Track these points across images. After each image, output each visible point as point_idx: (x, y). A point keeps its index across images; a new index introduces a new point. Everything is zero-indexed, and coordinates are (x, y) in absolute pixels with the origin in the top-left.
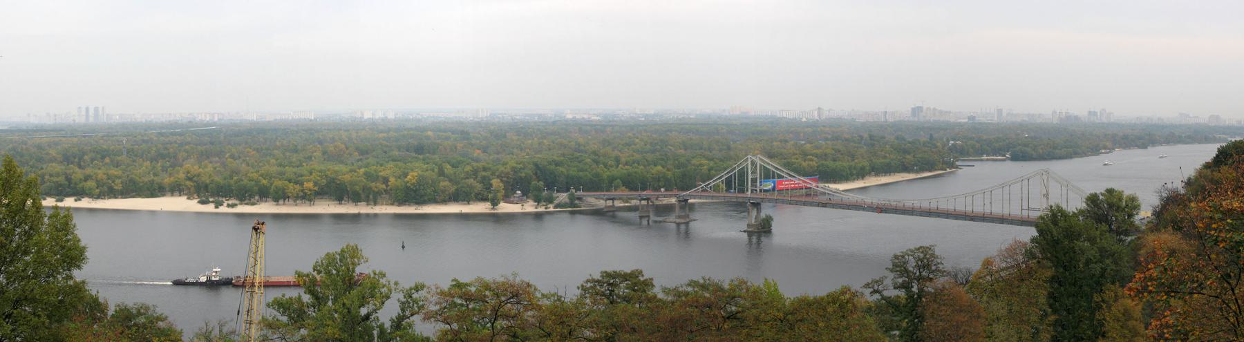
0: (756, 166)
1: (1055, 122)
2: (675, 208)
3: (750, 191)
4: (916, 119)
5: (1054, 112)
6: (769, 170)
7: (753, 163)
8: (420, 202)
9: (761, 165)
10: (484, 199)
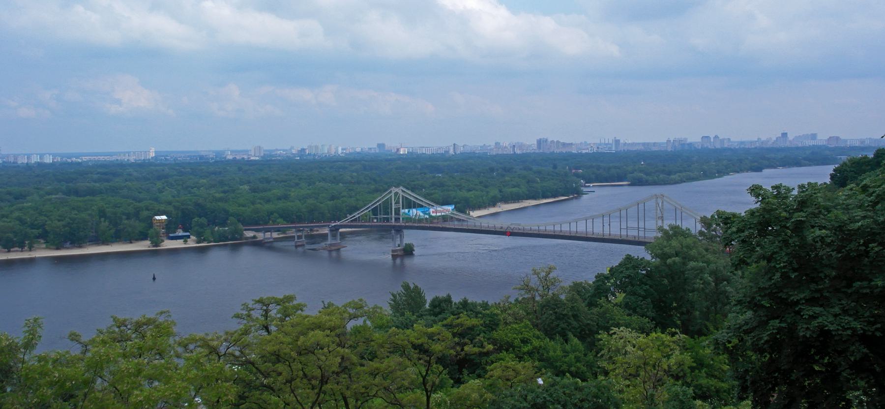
0: (399, 198)
1: (669, 149)
2: (328, 235)
3: (393, 219)
4: (541, 151)
5: (669, 141)
6: (411, 200)
8: (77, 242)
9: (403, 196)
10: (143, 237)
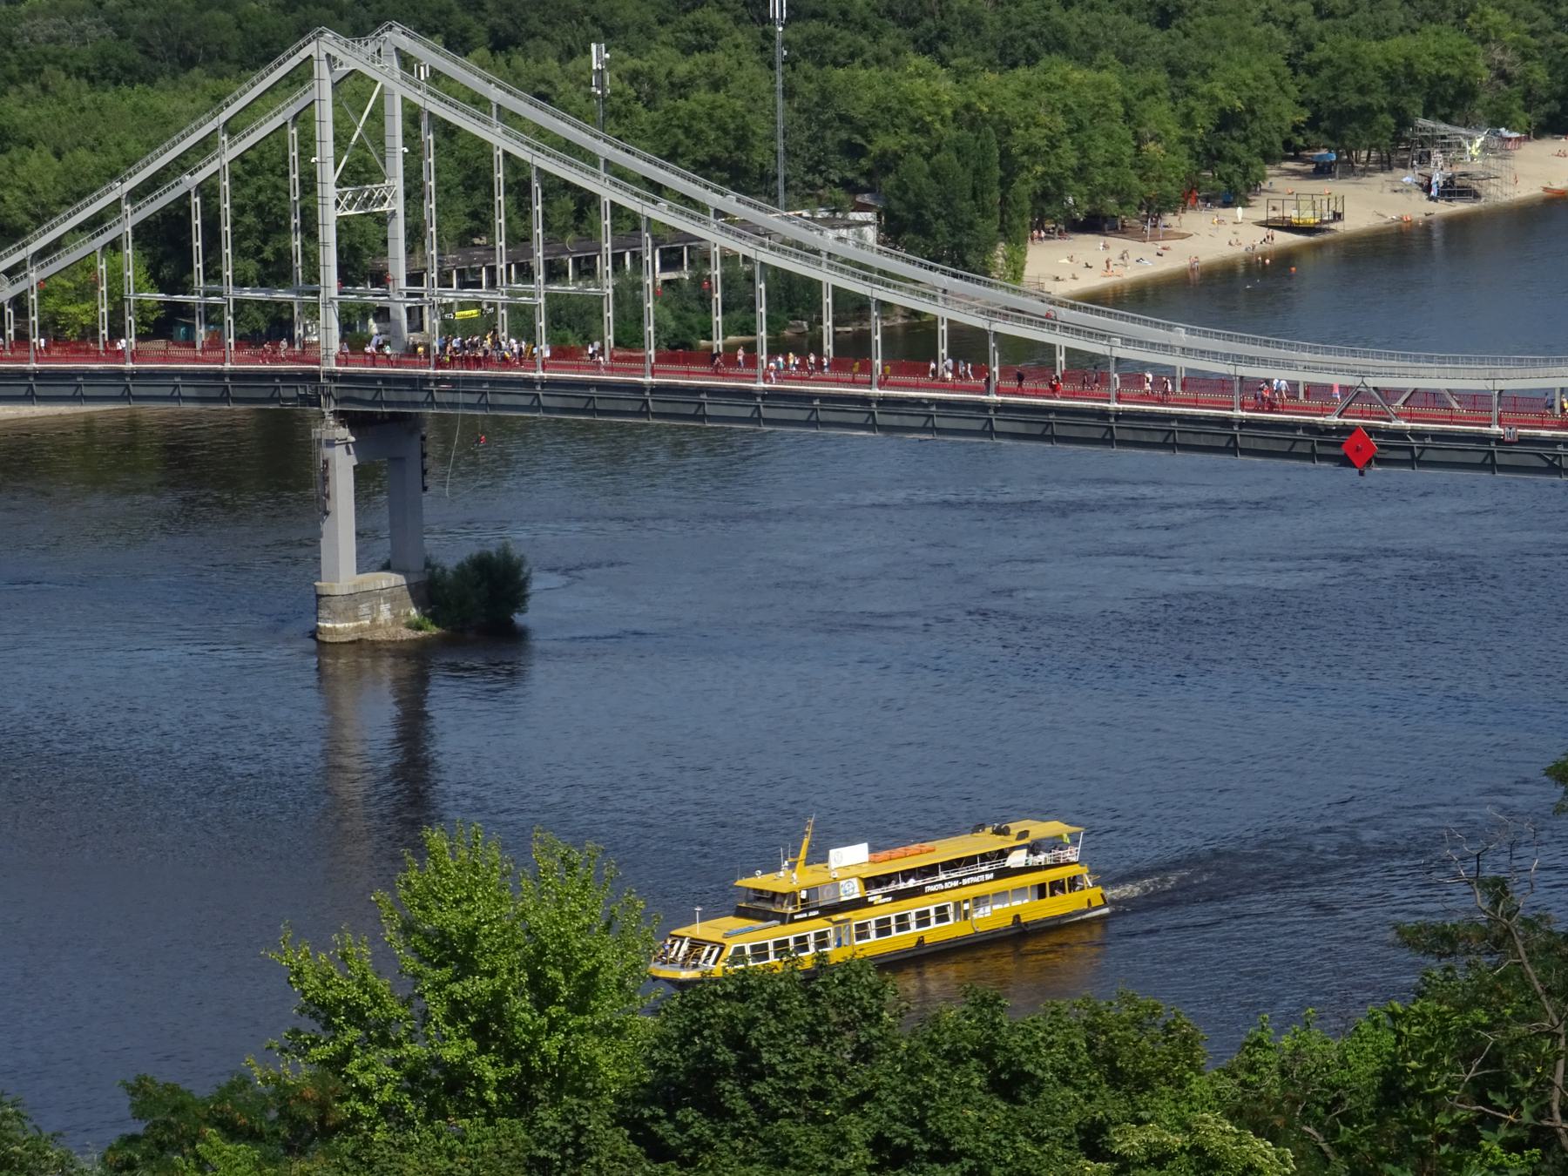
7: (353, 89)
